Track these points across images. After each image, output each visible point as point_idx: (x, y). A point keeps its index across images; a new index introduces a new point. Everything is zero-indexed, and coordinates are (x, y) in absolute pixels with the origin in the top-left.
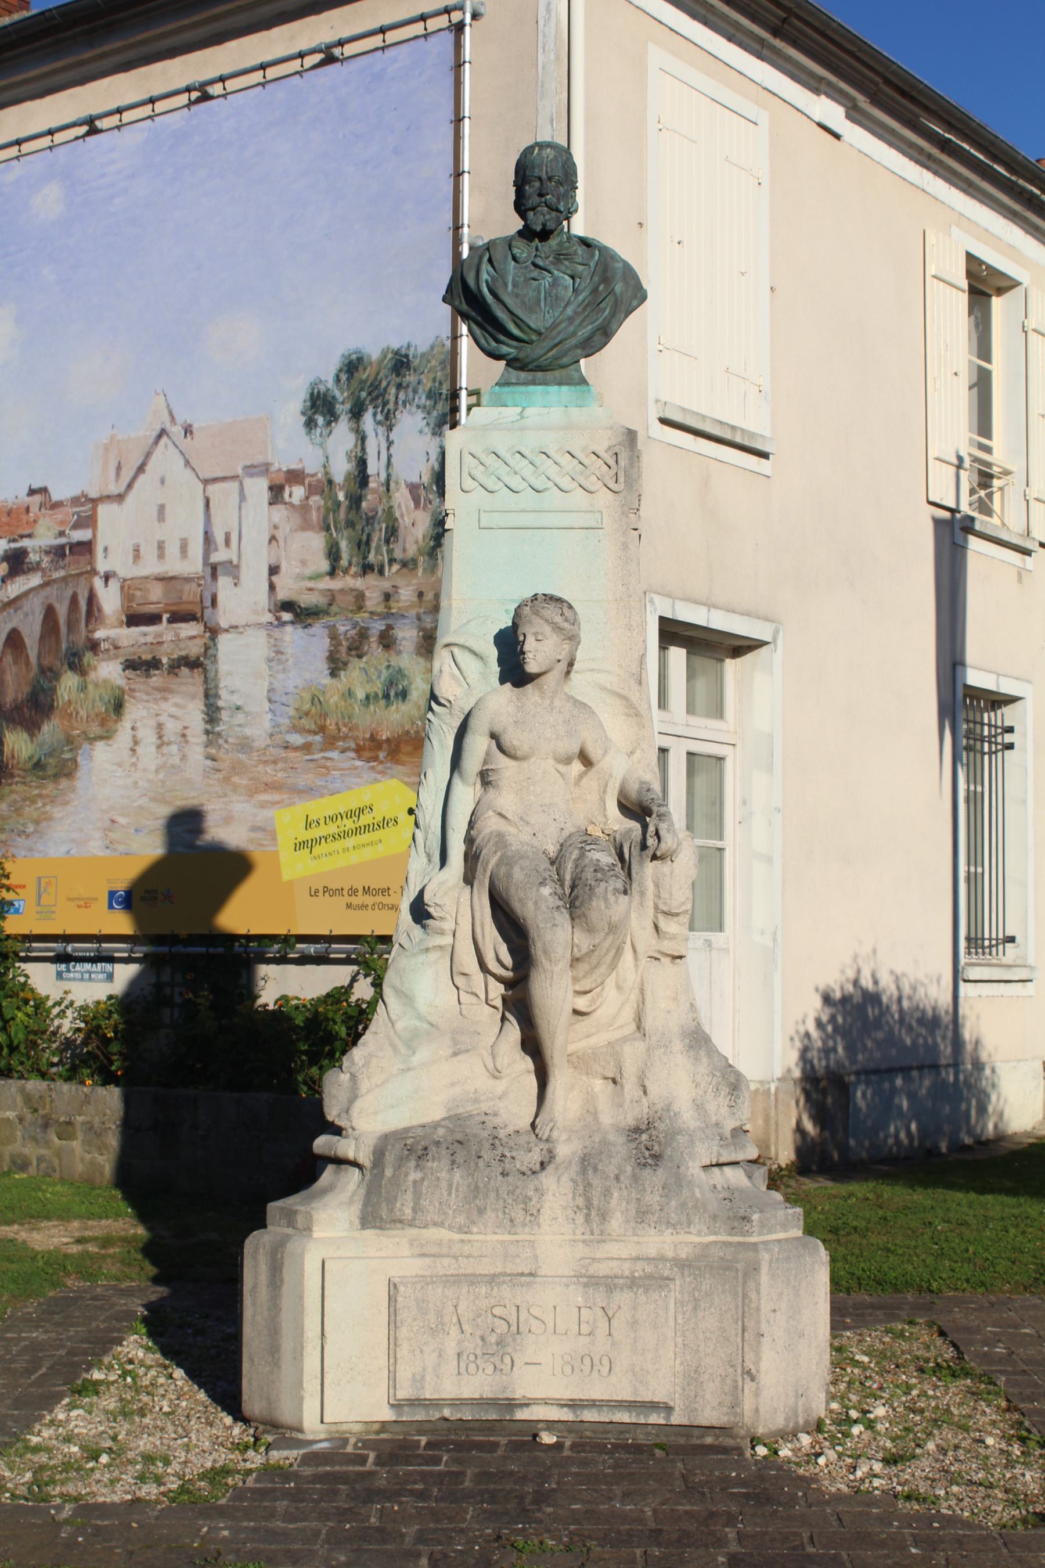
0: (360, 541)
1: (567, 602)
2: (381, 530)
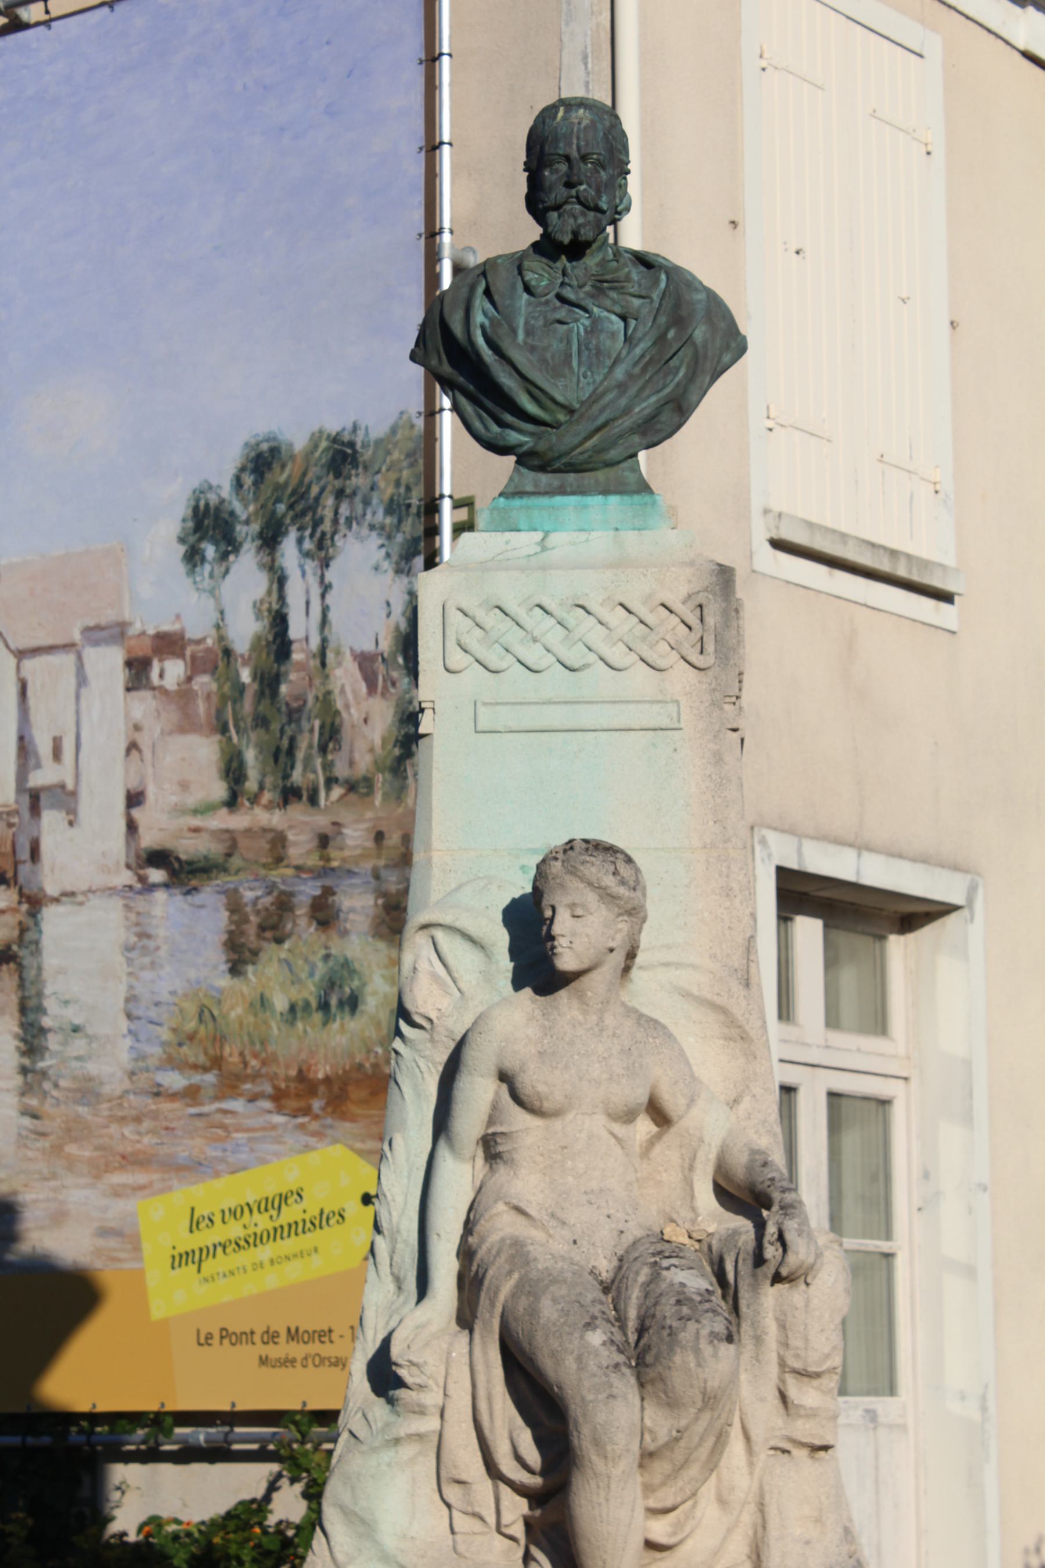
1: (622, 852)
2: (312, 730)
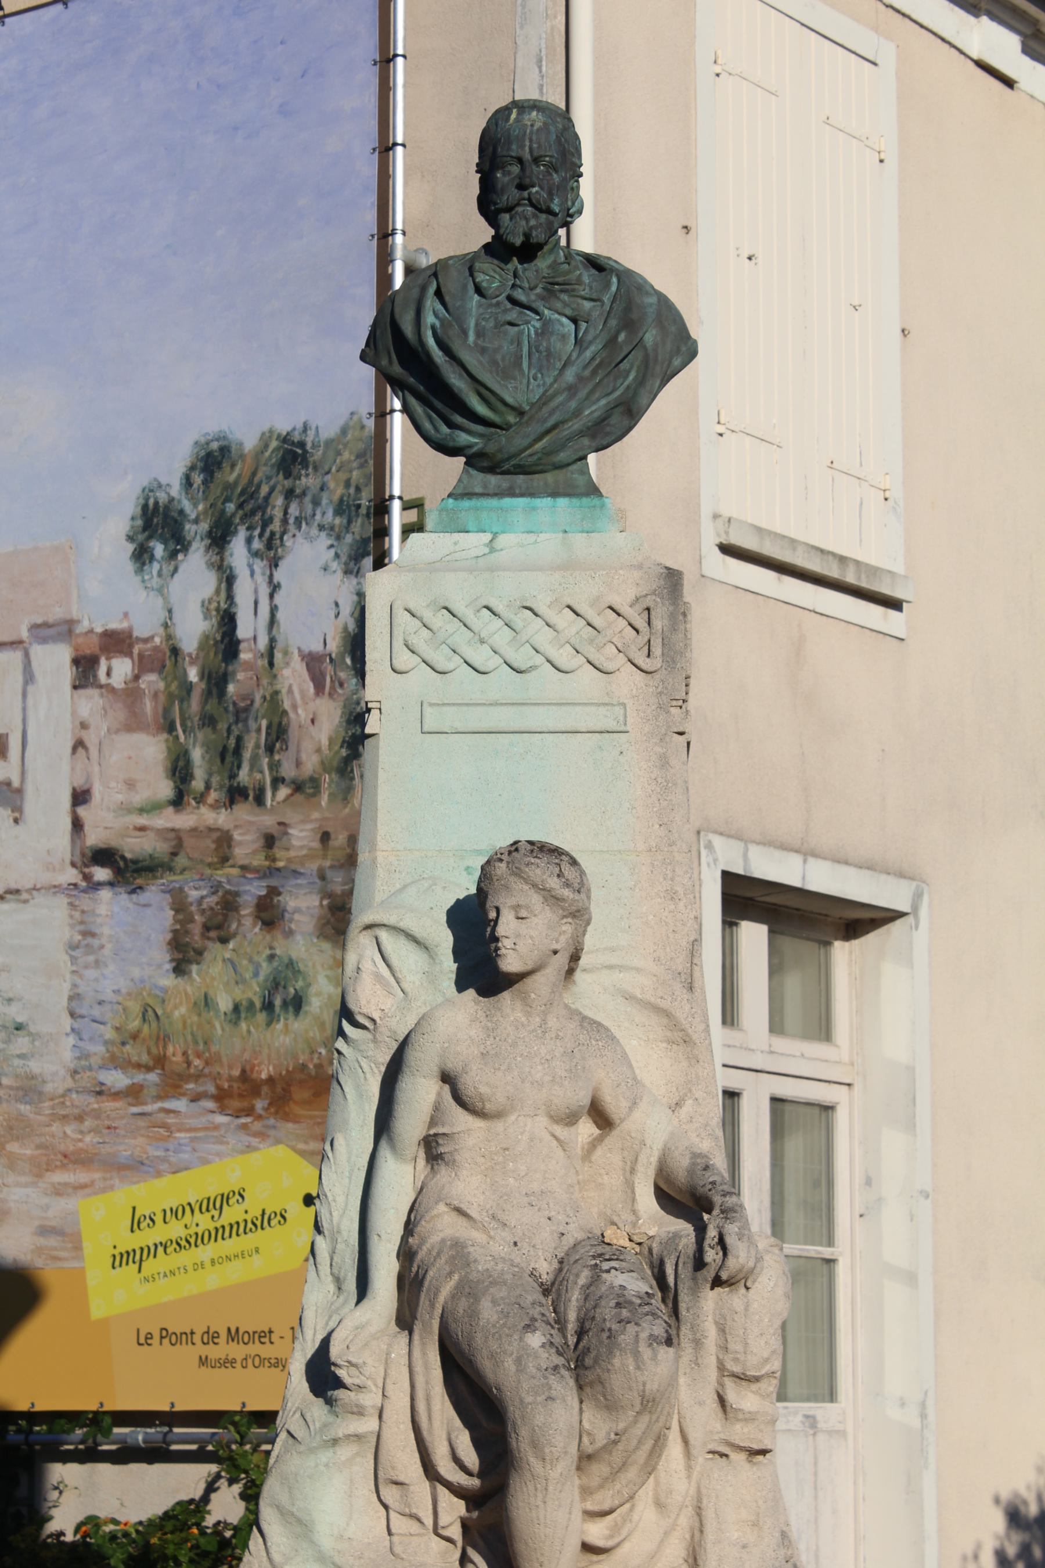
1: (567, 854)
2: (259, 730)
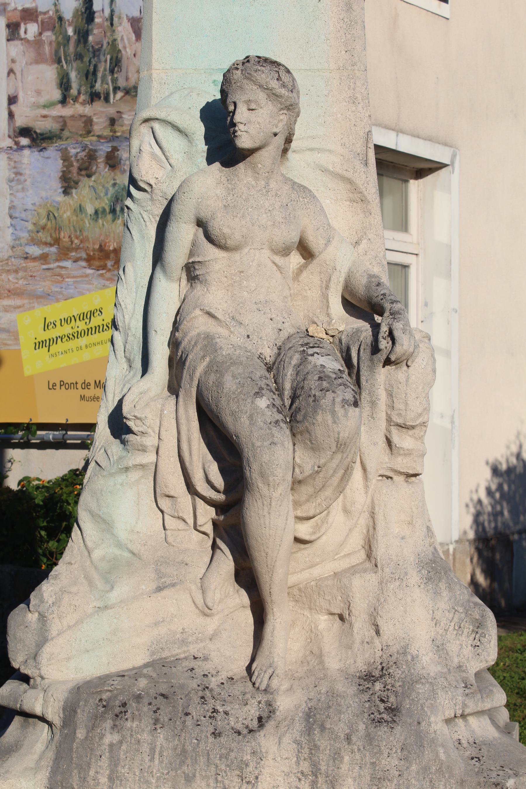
0: (88, 71)
1: (283, 66)
